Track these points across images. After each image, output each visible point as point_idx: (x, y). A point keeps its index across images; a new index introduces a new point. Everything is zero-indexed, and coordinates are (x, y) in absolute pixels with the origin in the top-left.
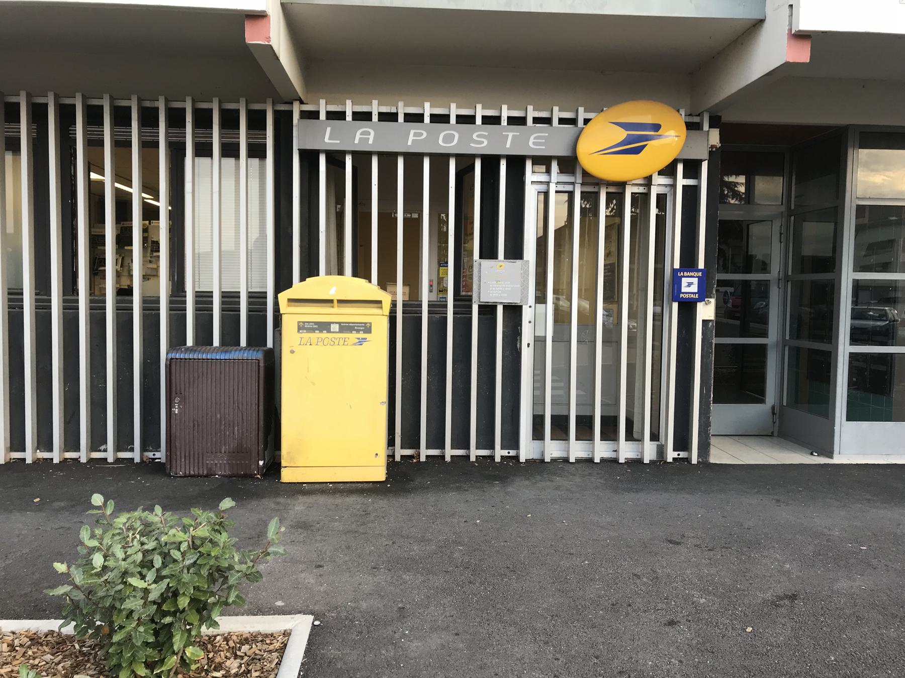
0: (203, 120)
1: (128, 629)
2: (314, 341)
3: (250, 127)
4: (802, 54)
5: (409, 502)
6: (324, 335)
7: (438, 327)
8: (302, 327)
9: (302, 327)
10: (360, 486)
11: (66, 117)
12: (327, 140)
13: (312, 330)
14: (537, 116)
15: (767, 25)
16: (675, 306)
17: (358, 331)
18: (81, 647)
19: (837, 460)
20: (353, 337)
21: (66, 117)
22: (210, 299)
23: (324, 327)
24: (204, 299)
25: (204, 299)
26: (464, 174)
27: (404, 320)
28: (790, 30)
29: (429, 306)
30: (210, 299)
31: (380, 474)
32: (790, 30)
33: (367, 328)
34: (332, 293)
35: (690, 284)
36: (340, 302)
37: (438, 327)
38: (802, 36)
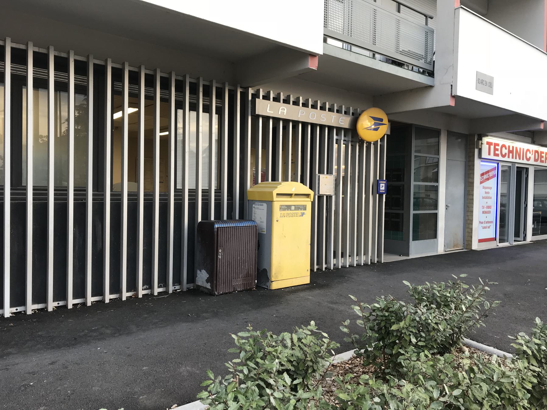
0: (41, 62)
1: (432, 324)
2: (285, 215)
3: (13, 61)
4: (452, 103)
5: (317, 292)
6: (289, 212)
7: (81, 207)
8: (283, 208)
9: (283, 208)
10: (296, 288)
11: (118, 76)
12: (268, 111)
13: (284, 210)
14: (131, 69)
15: (434, 89)
16: (378, 195)
17: (301, 209)
18: (366, 351)
19: (411, 256)
20: (300, 212)
21: (118, 76)
22: (24, 192)
23: (289, 207)
24: (179, 194)
25: (179, 194)
26: (285, 128)
27: (55, 205)
28: (451, 94)
29: (129, 195)
30: (24, 192)
31: (307, 280)
32: (451, 94)
33: (304, 208)
34: (293, 191)
35: (382, 186)
36: (296, 195)
37: (81, 207)
38: (455, 97)
